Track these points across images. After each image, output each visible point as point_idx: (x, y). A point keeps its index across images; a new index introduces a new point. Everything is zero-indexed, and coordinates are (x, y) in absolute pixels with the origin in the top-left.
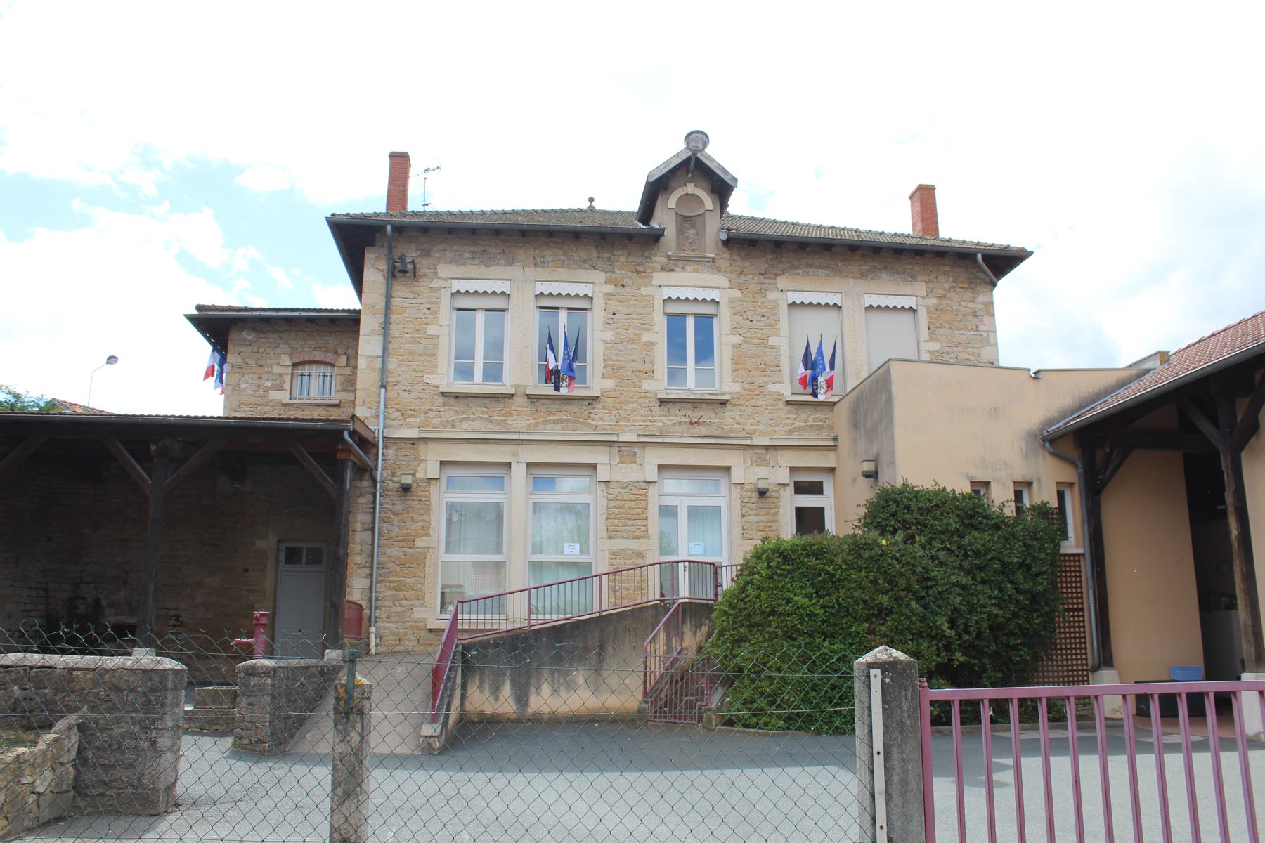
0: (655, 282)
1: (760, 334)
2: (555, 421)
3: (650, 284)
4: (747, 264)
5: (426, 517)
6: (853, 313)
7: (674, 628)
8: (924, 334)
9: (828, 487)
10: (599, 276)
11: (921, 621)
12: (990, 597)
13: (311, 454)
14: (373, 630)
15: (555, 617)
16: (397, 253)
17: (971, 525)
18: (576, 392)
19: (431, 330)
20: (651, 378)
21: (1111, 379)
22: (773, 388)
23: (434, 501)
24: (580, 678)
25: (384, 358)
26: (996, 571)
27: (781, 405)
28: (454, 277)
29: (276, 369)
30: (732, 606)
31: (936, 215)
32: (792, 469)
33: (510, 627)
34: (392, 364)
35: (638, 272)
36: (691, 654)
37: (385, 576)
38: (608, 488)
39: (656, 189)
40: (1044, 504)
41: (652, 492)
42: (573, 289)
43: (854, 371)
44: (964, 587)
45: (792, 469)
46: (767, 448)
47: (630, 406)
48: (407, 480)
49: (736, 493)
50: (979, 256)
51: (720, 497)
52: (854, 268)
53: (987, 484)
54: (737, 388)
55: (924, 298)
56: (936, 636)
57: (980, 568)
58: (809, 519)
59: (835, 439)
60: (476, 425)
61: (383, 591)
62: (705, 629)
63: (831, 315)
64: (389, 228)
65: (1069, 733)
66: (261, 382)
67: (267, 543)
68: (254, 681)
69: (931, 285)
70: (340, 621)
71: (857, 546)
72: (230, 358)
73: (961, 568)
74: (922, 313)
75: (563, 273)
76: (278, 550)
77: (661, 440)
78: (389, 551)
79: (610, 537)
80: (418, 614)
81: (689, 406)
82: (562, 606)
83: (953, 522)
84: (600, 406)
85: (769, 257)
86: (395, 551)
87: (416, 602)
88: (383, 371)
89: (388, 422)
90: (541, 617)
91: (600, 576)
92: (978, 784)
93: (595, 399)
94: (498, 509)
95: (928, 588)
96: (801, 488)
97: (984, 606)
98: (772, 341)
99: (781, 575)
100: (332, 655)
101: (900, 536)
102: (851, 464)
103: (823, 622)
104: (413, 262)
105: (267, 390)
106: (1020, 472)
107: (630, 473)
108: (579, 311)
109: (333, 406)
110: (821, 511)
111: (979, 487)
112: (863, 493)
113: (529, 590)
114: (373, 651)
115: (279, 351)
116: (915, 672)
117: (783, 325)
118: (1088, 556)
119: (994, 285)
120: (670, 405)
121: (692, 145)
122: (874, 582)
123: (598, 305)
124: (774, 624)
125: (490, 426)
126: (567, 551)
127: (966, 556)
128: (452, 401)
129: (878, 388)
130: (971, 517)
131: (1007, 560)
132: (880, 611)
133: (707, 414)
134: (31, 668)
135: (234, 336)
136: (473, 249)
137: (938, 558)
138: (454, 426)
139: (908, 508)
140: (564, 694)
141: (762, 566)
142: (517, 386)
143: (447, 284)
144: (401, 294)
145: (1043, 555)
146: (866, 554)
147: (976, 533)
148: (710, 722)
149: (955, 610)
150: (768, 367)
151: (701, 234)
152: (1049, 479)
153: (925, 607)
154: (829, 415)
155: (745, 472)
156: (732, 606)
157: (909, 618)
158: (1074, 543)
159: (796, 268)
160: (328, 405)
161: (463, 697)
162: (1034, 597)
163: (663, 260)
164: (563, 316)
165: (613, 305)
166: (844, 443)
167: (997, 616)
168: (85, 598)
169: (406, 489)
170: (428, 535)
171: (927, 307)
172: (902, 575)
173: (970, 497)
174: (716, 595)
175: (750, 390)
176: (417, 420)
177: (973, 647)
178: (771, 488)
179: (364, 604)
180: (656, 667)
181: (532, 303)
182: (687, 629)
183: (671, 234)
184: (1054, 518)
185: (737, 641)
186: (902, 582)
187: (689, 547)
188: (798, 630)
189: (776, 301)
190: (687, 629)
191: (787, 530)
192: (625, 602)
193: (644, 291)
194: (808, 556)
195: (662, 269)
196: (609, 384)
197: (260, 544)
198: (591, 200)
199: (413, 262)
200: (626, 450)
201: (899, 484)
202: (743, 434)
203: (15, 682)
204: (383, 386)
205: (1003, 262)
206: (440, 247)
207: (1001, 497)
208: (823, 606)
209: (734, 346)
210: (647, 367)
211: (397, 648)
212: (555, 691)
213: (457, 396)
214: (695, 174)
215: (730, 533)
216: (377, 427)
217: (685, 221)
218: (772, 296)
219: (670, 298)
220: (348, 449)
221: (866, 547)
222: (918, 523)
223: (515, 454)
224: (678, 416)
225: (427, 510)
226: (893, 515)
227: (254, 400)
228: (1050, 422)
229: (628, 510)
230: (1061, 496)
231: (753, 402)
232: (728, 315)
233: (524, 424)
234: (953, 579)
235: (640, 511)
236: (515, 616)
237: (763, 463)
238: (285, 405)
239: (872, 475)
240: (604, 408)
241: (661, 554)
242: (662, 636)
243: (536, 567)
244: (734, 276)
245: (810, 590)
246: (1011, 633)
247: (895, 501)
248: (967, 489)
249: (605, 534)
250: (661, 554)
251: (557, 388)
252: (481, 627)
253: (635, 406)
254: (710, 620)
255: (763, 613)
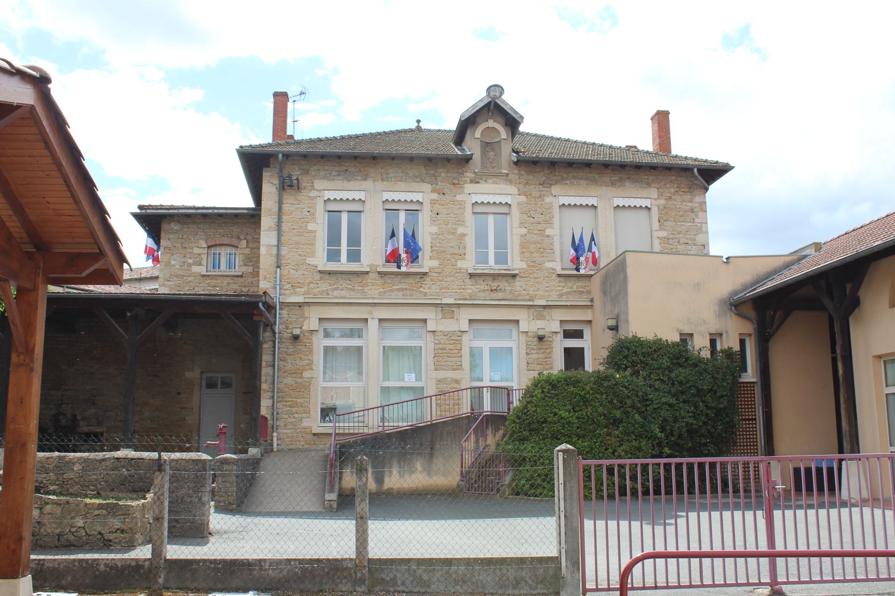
0: (466, 191)
1: (539, 227)
2: (398, 290)
3: (462, 192)
4: (531, 178)
5: (310, 357)
6: (606, 213)
7: (480, 432)
8: (656, 225)
9: (587, 334)
10: (427, 187)
11: (641, 428)
12: (688, 412)
13: (232, 314)
14: (275, 434)
15: (400, 424)
16: (286, 172)
17: (678, 364)
18: (412, 270)
19: (311, 227)
20: (464, 259)
21: (779, 262)
22: (548, 265)
23: (315, 346)
24: (419, 466)
25: (278, 246)
26: (693, 395)
27: (554, 276)
28: (328, 191)
29: (196, 251)
30: (519, 417)
31: (669, 133)
32: (562, 322)
33: (371, 431)
34: (284, 251)
35: (454, 184)
36: (492, 449)
37: (282, 397)
38: (434, 336)
39: (467, 124)
40: (730, 349)
41: (465, 338)
42: (409, 197)
43: (606, 254)
44: (671, 405)
45: (562, 322)
46: (544, 307)
47: (449, 279)
48: (297, 332)
49: (523, 338)
50: (695, 170)
51: (513, 342)
52: (606, 179)
53: (692, 335)
54: (523, 265)
55: (656, 199)
56: (651, 437)
57: (683, 393)
58: (574, 357)
59: (592, 300)
60: (343, 293)
61: (282, 408)
62: (501, 432)
63: (589, 213)
64: (280, 156)
65: (741, 500)
66: (185, 259)
67: (193, 374)
68: (226, 467)
69: (661, 191)
70: (252, 428)
71: (600, 378)
72: (162, 243)
73: (669, 393)
74: (655, 211)
75: (402, 185)
76: (201, 379)
77: (471, 302)
78: (285, 381)
79: (436, 370)
80: (306, 423)
81: (490, 278)
82: (405, 417)
83: (665, 362)
84: (428, 279)
85: (546, 172)
86: (289, 381)
87: (304, 415)
88: (278, 256)
89: (282, 292)
90: (391, 424)
91: (430, 397)
92: (660, 524)
93: (425, 274)
94: (359, 349)
95: (647, 406)
96: (568, 334)
97: (683, 418)
98: (548, 232)
99: (550, 397)
100: (253, 451)
101: (629, 371)
102: (602, 321)
103: (578, 428)
104: (297, 179)
105: (190, 265)
106: (714, 326)
107: (449, 326)
108: (413, 213)
109: (237, 276)
110: (582, 350)
111: (685, 338)
112: (608, 340)
113: (383, 407)
114: (275, 450)
115: (198, 237)
116: (576, 454)
117: (556, 220)
118: (759, 384)
119: (707, 189)
120: (477, 278)
121: (492, 94)
122: (611, 402)
123: (427, 207)
124: (546, 429)
125: (353, 293)
126: (406, 379)
127: (673, 384)
128: (326, 277)
129: (619, 266)
130: (678, 358)
131: (700, 387)
132: (615, 421)
133: (503, 284)
134: (132, 459)
135: (165, 226)
136: (338, 168)
137: (654, 386)
138: (328, 294)
139: (635, 352)
140: (407, 477)
141: (538, 392)
142: (371, 266)
143: (321, 194)
144: (289, 202)
145: (725, 384)
146: (606, 384)
147: (680, 369)
148: (504, 493)
149: (665, 420)
150: (545, 250)
151: (498, 154)
152: (734, 332)
153: (645, 418)
154: (588, 284)
155: (529, 324)
156: (519, 417)
157: (633, 425)
158: (750, 375)
159: (566, 179)
160: (234, 276)
161: (340, 479)
162: (718, 412)
163: (471, 175)
164: (402, 215)
165: (437, 207)
166: (598, 303)
167: (692, 424)
168: (65, 415)
169: (296, 338)
170: (312, 369)
171: (658, 206)
172: (629, 397)
173: (677, 344)
174: (509, 409)
175: (532, 266)
176: (303, 290)
177: (678, 444)
178: (547, 335)
179: (269, 417)
180: (469, 459)
181: (380, 207)
182: (489, 432)
183: (477, 157)
184: (737, 360)
185: (522, 440)
186: (629, 402)
187: (490, 377)
188: (561, 433)
189: (551, 203)
190: (489, 432)
191: (558, 364)
192: (448, 414)
193: (459, 198)
194: (567, 385)
195: (471, 182)
196: (435, 263)
197: (188, 375)
198: (419, 121)
199: (297, 179)
200: (447, 310)
201: (630, 336)
202: (528, 297)
203: (124, 467)
204: (278, 267)
205: (712, 173)
206: (315, 168)
207: (700, 344)
208: (578, 418)
209: (522, 236)
210: (461, 251)
211: (292, 447)
212: (401, 475)
213: (330, 273)
214: (494, 111)
215: (518, 366)
216: (276, 297)
217: (487, 146)
218: (548, 200)
219: (476, 202)
220: (261, 314)
221: (607, 378)
222: (642, 362)
223: (370, 313)
224: (483, 285)
225: (311, 352)
226: (626, 357)
227: (180, 272)
228: (735, 293)
229: (448, 350)
230: (742, 342)
231: (534, 275)
232: (518, 213)
233: (377, 292)
234: (664, 400)
235: (456, 351)
236: (372, 424)
237: (541, 317)
238: (203, 276)
239: (614, 329)
240: (431, 280)
241: (471, 381)
242: (472, 436)
243: (385, 390)
244: (521, 186)
245: (569, 407)
246: (702, 435)
247: (627, 348)
248: (676, 338)
249: (433, 367)
250: (471, 381)
251: (399, 267)
252: (351, 431)
253: (452, 278)
254: (505, 426)
255: (538, 422)
